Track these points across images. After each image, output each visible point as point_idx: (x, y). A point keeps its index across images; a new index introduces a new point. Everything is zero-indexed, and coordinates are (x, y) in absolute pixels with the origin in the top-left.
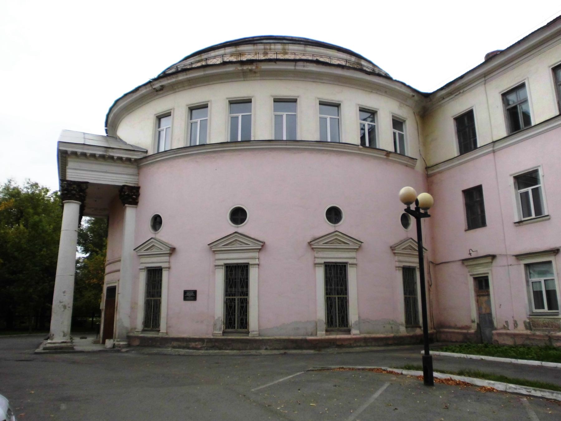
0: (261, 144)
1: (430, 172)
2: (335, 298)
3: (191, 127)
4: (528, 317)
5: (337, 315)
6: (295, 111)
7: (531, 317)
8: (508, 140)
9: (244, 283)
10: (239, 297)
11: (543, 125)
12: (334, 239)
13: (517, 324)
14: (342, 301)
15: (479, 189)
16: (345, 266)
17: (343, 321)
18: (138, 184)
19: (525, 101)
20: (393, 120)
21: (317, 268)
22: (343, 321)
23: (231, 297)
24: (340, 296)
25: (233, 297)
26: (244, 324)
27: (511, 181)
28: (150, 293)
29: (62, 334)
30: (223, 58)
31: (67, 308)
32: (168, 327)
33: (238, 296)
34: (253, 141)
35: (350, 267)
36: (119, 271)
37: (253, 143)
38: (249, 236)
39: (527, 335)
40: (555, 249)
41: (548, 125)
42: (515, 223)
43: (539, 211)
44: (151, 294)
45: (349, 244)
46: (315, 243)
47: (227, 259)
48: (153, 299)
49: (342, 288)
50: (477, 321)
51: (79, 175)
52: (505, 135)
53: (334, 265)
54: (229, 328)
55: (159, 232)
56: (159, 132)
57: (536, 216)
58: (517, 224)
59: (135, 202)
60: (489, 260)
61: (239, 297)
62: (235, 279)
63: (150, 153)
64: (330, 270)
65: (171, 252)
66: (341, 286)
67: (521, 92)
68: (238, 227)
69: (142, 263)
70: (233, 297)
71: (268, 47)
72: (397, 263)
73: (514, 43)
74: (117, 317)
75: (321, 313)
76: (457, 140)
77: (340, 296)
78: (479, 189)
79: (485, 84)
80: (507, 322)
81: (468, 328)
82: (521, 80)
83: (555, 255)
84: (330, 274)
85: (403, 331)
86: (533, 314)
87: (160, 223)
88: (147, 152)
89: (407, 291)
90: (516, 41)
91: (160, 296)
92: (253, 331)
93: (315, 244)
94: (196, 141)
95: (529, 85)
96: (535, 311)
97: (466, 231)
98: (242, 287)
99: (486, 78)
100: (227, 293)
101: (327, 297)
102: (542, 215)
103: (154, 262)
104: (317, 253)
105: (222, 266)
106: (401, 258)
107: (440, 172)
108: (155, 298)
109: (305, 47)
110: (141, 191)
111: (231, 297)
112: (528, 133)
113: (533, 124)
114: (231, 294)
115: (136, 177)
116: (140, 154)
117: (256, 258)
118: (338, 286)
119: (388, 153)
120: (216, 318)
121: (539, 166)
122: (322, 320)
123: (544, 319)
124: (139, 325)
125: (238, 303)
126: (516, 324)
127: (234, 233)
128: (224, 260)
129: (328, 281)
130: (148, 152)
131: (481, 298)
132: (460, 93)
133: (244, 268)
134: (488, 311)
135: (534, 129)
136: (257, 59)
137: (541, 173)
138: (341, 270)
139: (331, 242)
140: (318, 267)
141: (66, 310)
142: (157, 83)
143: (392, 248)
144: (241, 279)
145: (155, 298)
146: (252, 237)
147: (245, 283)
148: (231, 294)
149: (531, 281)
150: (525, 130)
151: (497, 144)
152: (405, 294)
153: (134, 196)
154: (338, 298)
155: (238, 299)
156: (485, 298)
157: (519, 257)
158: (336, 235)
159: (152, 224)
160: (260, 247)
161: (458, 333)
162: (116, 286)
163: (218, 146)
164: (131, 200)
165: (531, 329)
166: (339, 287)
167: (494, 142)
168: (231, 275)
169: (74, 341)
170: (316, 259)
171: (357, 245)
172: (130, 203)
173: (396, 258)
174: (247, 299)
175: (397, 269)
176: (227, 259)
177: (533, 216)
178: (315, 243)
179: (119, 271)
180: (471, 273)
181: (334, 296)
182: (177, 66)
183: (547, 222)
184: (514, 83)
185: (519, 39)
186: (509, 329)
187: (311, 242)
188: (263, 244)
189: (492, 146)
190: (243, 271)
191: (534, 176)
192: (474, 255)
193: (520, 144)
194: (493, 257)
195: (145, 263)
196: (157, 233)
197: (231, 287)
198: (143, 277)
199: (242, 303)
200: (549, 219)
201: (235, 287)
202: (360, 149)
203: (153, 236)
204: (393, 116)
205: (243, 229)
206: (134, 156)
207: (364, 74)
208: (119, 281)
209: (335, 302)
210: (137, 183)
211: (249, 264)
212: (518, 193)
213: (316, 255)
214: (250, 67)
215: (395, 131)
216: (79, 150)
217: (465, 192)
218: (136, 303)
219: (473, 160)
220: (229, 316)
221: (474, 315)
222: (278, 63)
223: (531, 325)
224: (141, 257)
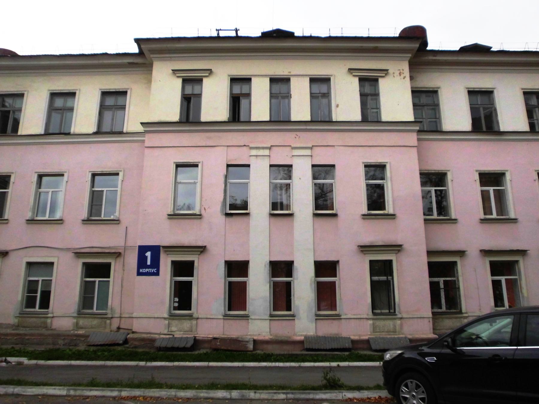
8: (432, 134)
11: (29, 138)
19: (20, 110)
40: (4, 252)
41: (31, 139)
67: (18, 101)
73: (27, 55)
82: (21, 90)
83: (3, 257)
86: (23, 313)
90: (30, 54)
95: (130, 98)
96: (25, 310)
102: (2, 218)
105: (250, 92)
112: (13, 140)
113: (19, 133)
121: (13, 173)
128: (259, 76)
135: (18, 138)
137: (12, 179)
149: (173, 279)
150: (9, 136)
169: (323, 375)
183: (60, 225)
184: (15, 90)
185: (33, 54)
191: (7, 179)
193: (99, 144)
200: (7, 223)
212: (91, 189)
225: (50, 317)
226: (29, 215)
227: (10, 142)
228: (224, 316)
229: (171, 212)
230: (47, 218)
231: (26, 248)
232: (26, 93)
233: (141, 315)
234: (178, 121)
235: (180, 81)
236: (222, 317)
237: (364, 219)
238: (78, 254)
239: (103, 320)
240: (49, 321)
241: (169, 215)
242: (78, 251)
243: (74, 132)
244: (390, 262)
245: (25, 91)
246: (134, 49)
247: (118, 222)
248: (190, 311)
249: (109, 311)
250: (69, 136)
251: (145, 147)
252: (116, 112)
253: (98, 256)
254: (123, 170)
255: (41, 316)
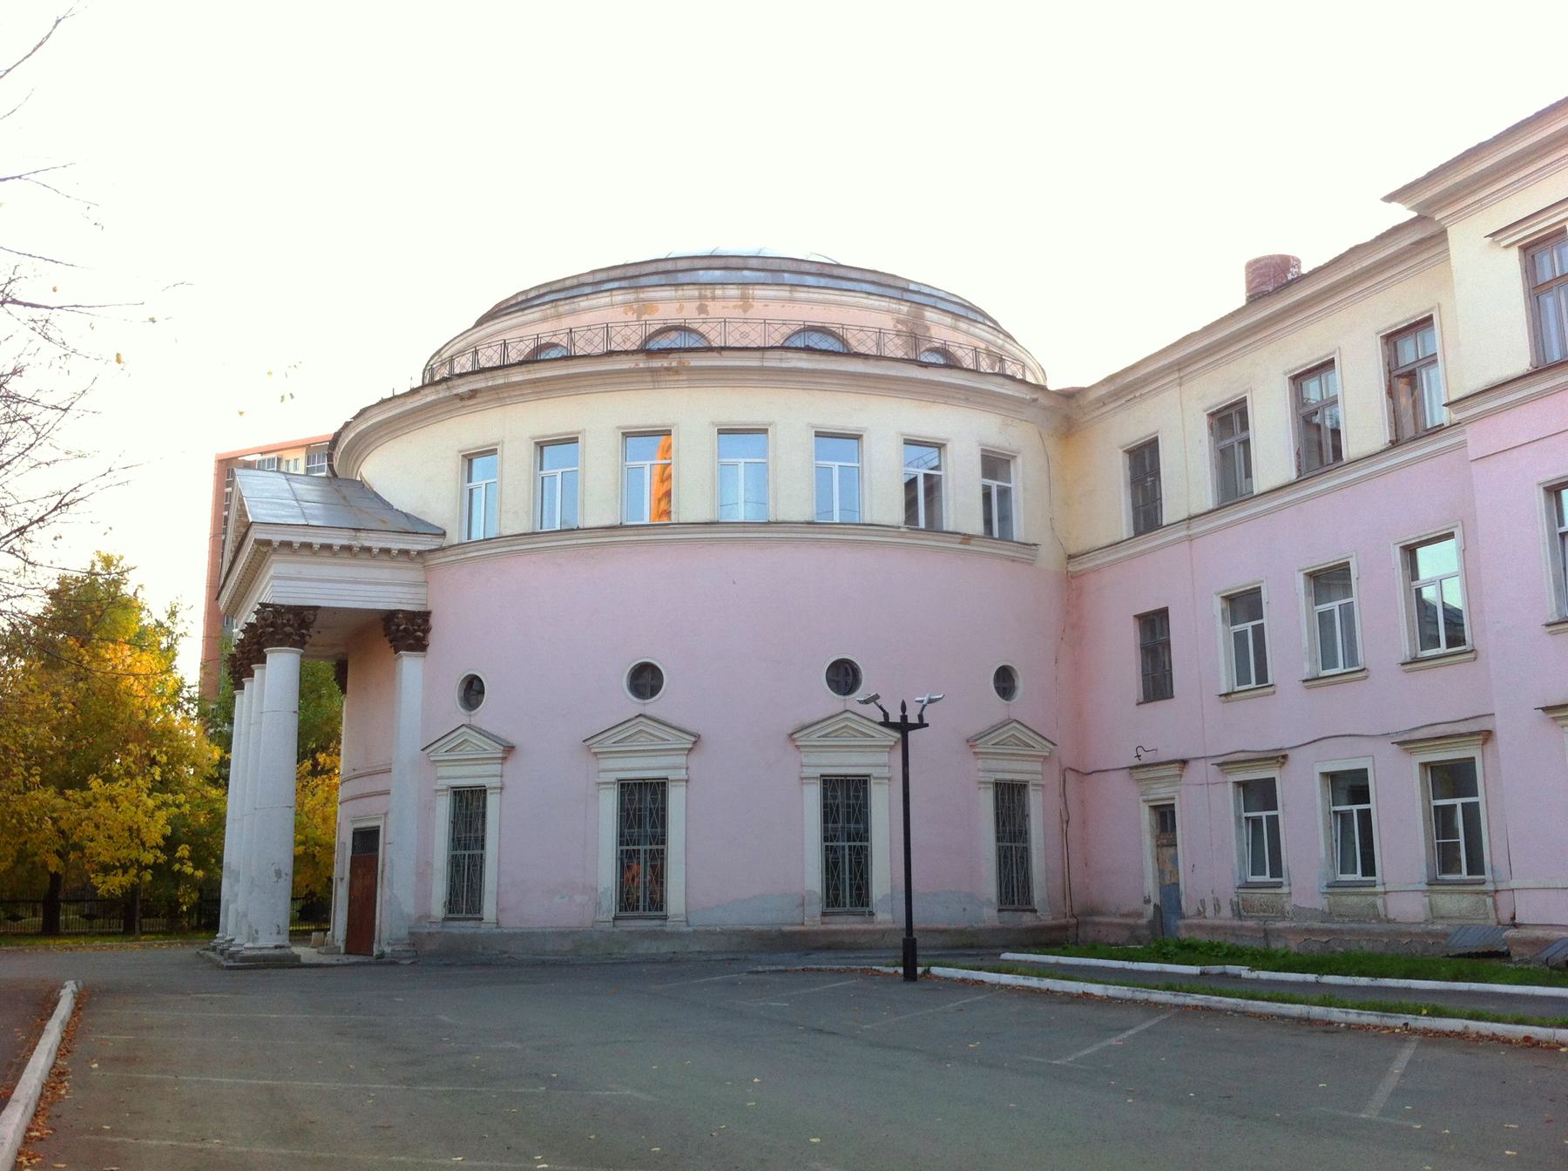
0: (693, 530)
1: (1074, 567)
2: (843, 847)
3: (541, 488)
4: (1325, 890)
5: (847, 881)
6: (764, 453)
7: (1240, 891)
9: (658, 819)
10: (648, 847)
12: (843, 727)
13: (1219, 908)
14: (858, 853)
15: (1163, 613)
16: (865, 782)
17: (859, 896)
18: (426, 605)
20: (983, 456)
21: (805, 787)
22: (859, 896)
23: (631, 847)
24: (852, 844)
25: (636, 847)
26: (657, 903)
27: (1218, 605)
28: (459, 839)
29: (275, 930)
30: (608, 330)
31: (283, 875)
32: (500, 910)
33: (644, 845)
34: (676, 524)
35: (875, 783)
36: (387, 793)
37: (674, 528)
38: (668, 721)
39: (1233, 928)
42: (1220, 696)
43: (1262, 676)
44: (462, 842)
45: (873, 737)
46: (802, 736)
47: (622, 770)
48: (467, 853)
49: (857, 826)
50: (1156, 899)
51: (307, 590)
52: (1210, 503)
53: (842, 780)
54: (626, 910)
55: (476, 713)
56: (471, 490)
57: (1257, 684)
58: (1223, 698)
59: (420, 645)
60: (1174, 770)
61: (648, 847)
62: (640, 810)
63: (454, 537)
64: (834, 790)
65: (505, 756)
66: (857, 822)
68: (645, 704)
69: (442, 778)
70: (636, 847)
71: (708, 293)
72: (981, 774)
74: (383, 895)
75: (813, 879)
76: (1130, 500)
77: (852, 844)
78: (1163, 613)
79: (1180, 385)
80: (1202, 902)
81: (1140, 915)
82: (1238, 391)
84: (835, 798)
85: (989, 916)
87: (481, 692)
88: (444, 534)
89: (1004, 832)
91: (483, 847)
92: (675, 915)
93: (802, 739)
94: (552, 519)
97: (1139, 704)
98: (654, 826)
99: (1182, 374)
100: (623, 839)
101: (827, 847)
103: (467, 776)
104: (805, 756)
106: (993, 764)
107: (1097, 569)
108: (471, 852)
109: (791, 291)
110: (433, 621)
111: (631, 847)
114: (631, 840)
115: (422, 590)
116: (429, 539)
117: (681, 768)
118: (849, 822)
119: (967, 538)
120: (601, 890)
122: (815, 892)
123: (1259, 895)
124: (438, 908)
125: (645, 858)
126: (1217, 908)
127: (637, 717)
129: (829, 813)
130: (448, 535)
131: (1165, 849)
132: (1135, 397)
133: (658, 788)
134: (1173, 880)
136: (683, 346)
138: (857, 790)
139: (836, 734)
140: (806, 783)
141: (281, 880)
142: (463, 384)
143: (972, 742)
144: (651, 809)
145: (471, 852)
146: (675, 723)
147: (660, 817)
148: (631, 840)
151: (1195, 523)
152: (998, 839)
153: (419, 633)
154: (850, 847)
155: (645, 850)
156: (1171, 850)
157: (1226, 765)
158: (847, 718)
159: (462, 694)
160: (690, 746)
161: (1119, 925)
162: (379, 827)
163: (604, 534)
164: (411, 641)
165: (1240, 917)
166: (852, 826)
167: (1190, 518)
168: (631, 801)
170: (805, 769)
171: (891, 738)
172: (411, 648)
173: (980, 764)
174: (663, 850)
175: (982, 786)
176: (622, 770)
177: (1253, 684)
178: (802, 736)
179: (387, 793)
180: (1145, 797)
181: (840, 844)
182: (505, 341)
186: (1205, 917)
187: (792, 734)
188: (697, 738)
189: (1185, 526)
190: (654, 793)
192: (1147, 758)
194: (1184, 762)
195: (449, 778)
196: (474, 715)
197: (631, 827)
198: (443, 808)
199: (653, 858)
201: (640, 827)
202: (902, 535)
203: (465, 721)
204: (983, 450)
205: (653, 706)
206: (415, 544)
207: (916, 367)
208: (386, 814)
209: (844, 855)
210: (425, 602)
211: (667, 779)
213: (805, 760)
214: (665, 363)
215: (988, 482)
216: (297, 539)
217: (1139, 617)
218: (429, 864)
219: (1531, 308)
220: (832, 880)
221: (1151, 887)
222: (725, 353)
223: (1240, 907)
224: (437, 764)
225: (1381, 893)
226: (1307, 670)
227: (1324, 486)
228: (1429, 884)
229: (1551, 616)
230: (1340, 669)
231: (1315, 741)
232: (1248, 395)
233: (1530, 883)
234: (1530, 368)
235: (1514, 253)
236: (1425, 887)
237: (1308, 688)
238: (1407, 744)
239: (1480, 896)
240: (1379, 902)
241: (1548, 625)
242: (1406, 737)
243: (1348, 458)
244: (1273, 780)
245: (1246, 391)
246: (1402, 213)
247: (1472, 655)
248: (1263, 877)
249: (1488, 876)
250: (1443, 434)
251: (1471, 461)
252: (1428, 374)
253: (1428, 746)
254: (1354, 553)
255: (1363, 890)
